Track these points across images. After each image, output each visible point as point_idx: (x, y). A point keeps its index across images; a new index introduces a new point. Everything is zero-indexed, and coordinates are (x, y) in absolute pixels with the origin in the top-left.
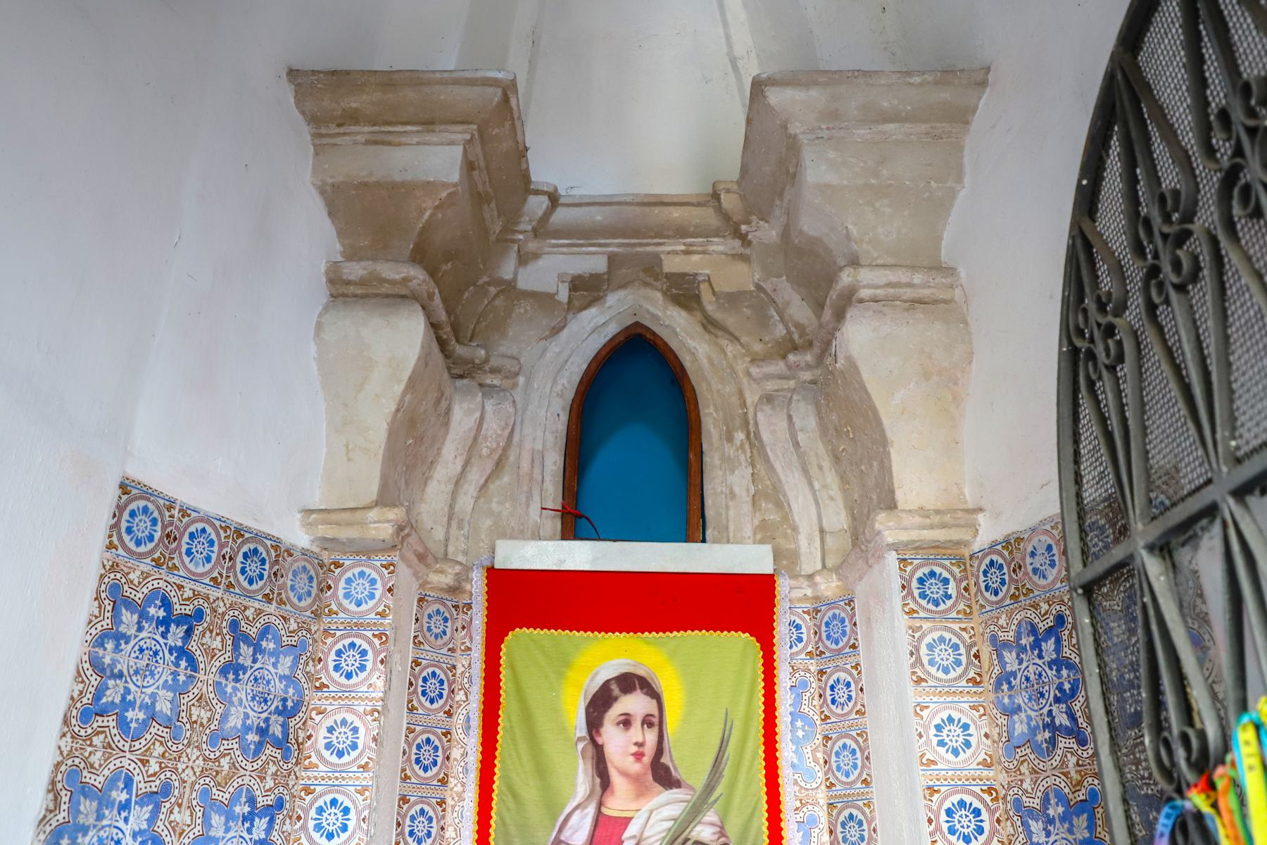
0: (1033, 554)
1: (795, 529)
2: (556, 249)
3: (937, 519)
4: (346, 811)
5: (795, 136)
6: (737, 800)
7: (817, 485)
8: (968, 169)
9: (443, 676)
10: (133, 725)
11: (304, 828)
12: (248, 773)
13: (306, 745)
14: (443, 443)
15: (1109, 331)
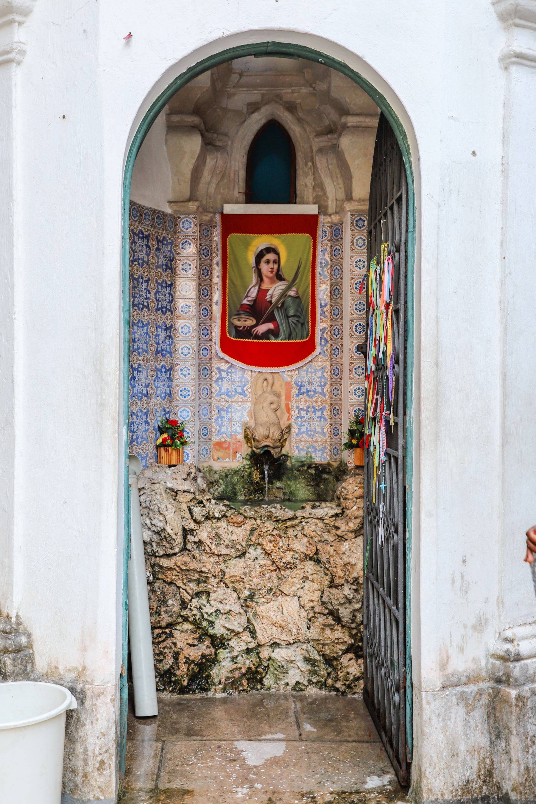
1: (327, 198)
6: (302, 284)
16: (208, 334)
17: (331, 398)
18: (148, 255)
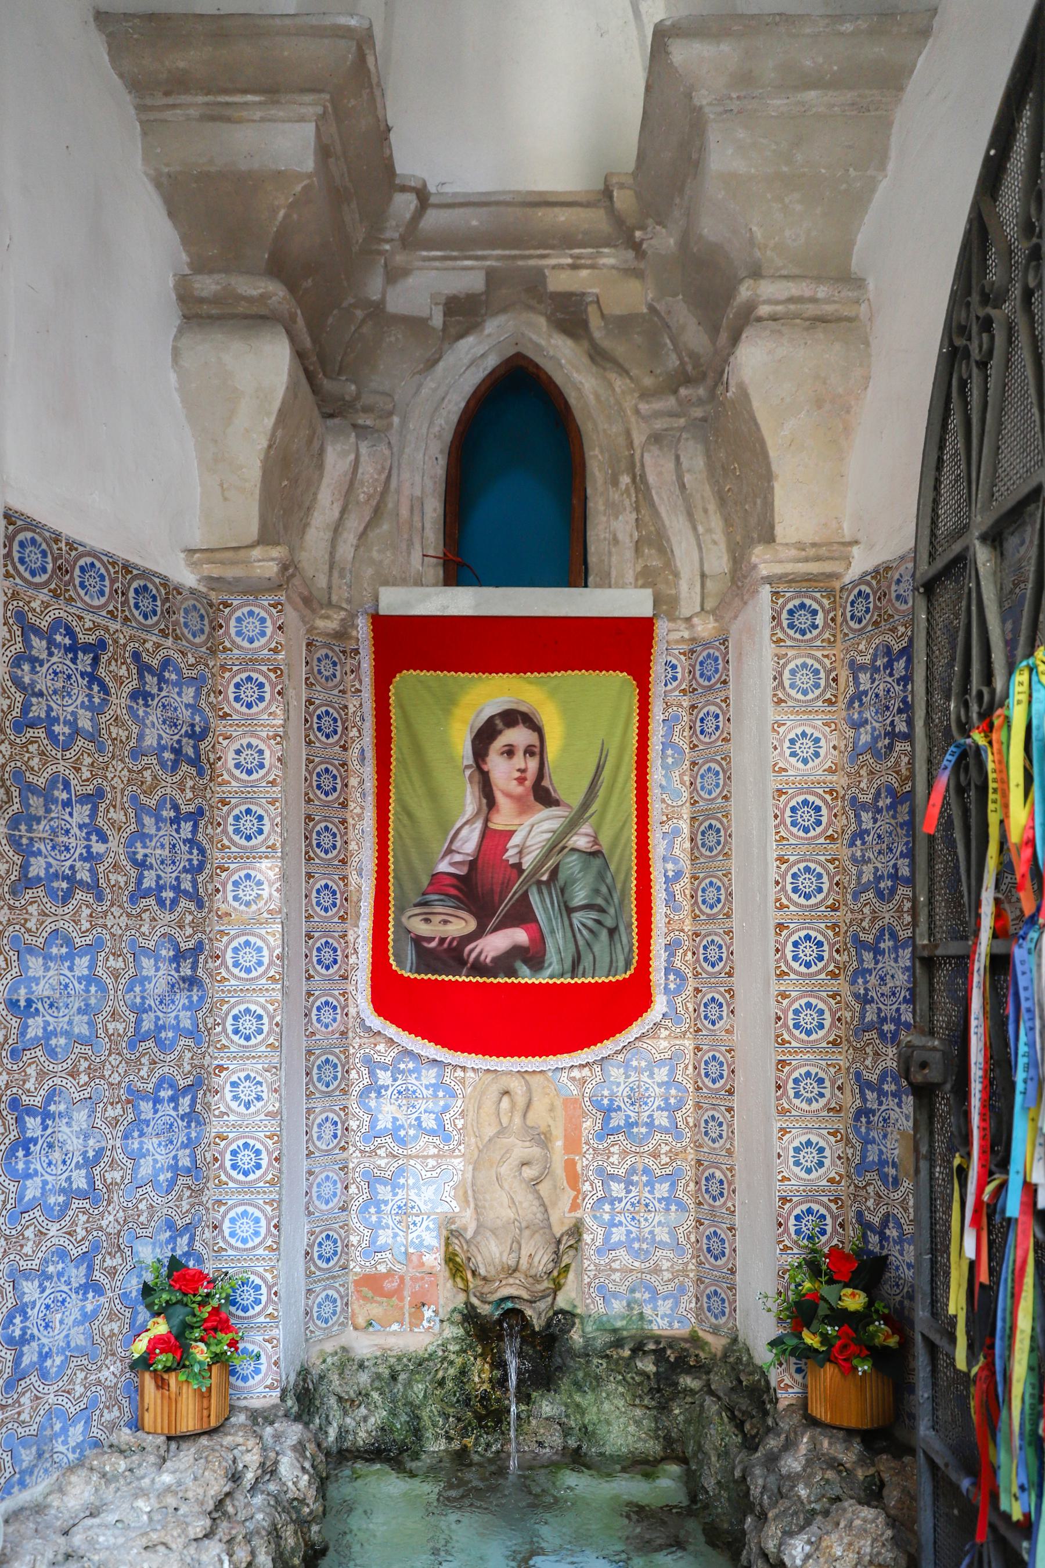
0: (899, 582)
1: (676, 575)
2: (427, 264)
3: (812, 552)
4: (260, 818)
5: (701, 108)
6: (609, 816)
7: (701, 529)
8: (893, 153)
9: (335, 715)
10: (61, 738)
14: (318, 488)
15: (987, 324)
16: (335, 962)
17: (698, 1146)
18: (97, 711)
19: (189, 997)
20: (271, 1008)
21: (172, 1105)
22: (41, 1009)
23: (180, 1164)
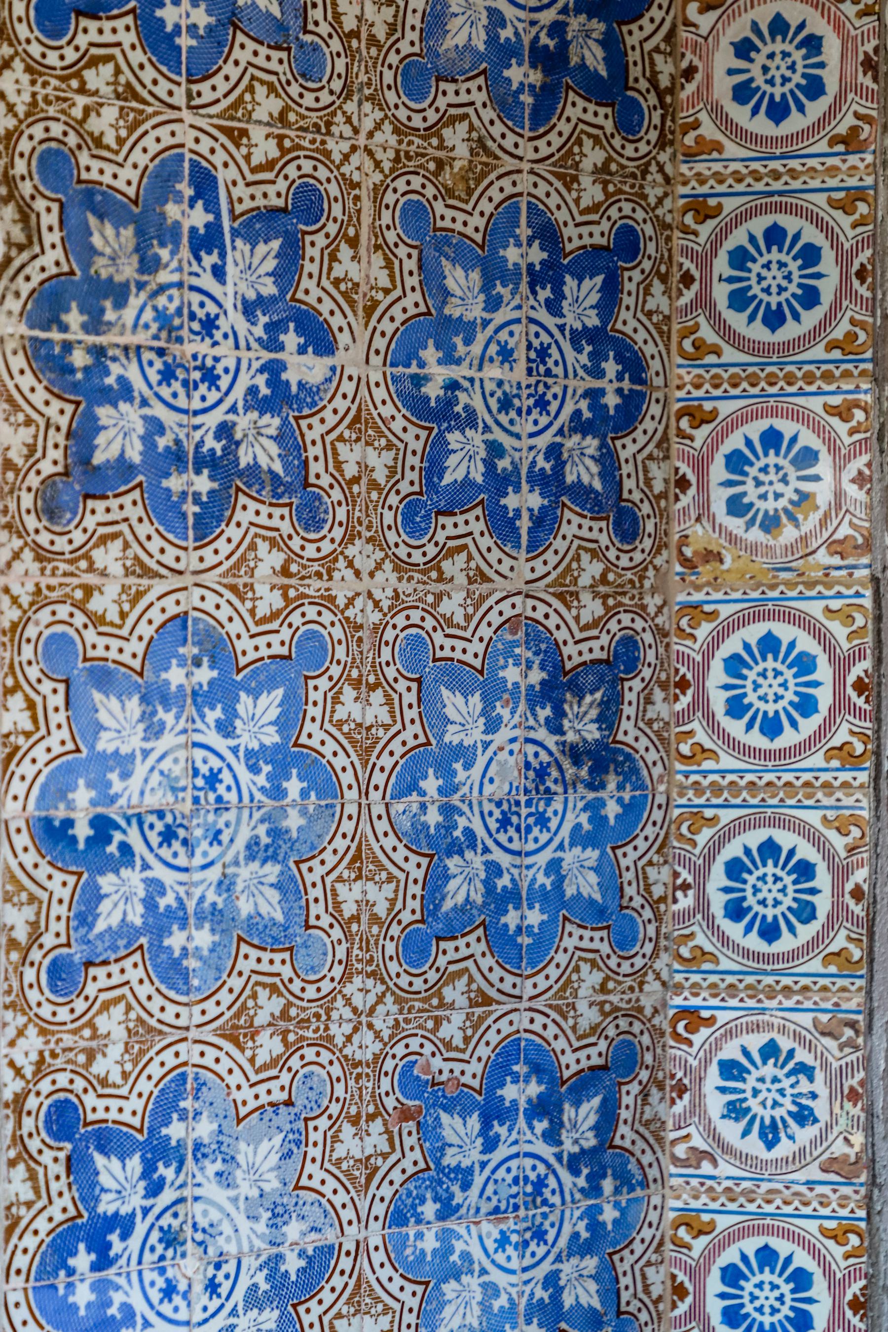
10: (185, 41)
11: (704, 301)
12: (526, 166)
13: (683, 95)
19: (594, 808)
20: (839, 843)
21: (541, 1126)
22: (138, 846)
23: (568, 1300)
